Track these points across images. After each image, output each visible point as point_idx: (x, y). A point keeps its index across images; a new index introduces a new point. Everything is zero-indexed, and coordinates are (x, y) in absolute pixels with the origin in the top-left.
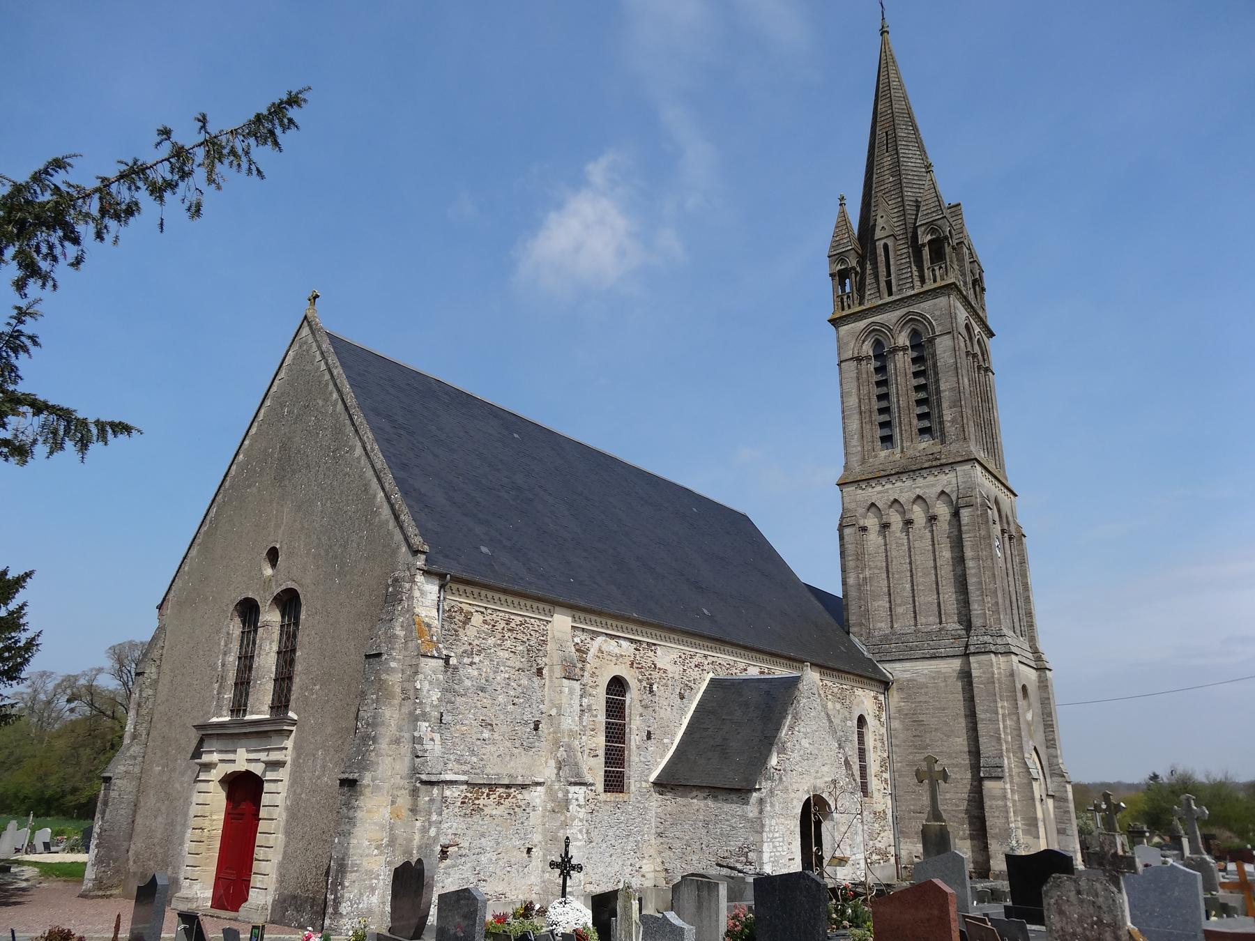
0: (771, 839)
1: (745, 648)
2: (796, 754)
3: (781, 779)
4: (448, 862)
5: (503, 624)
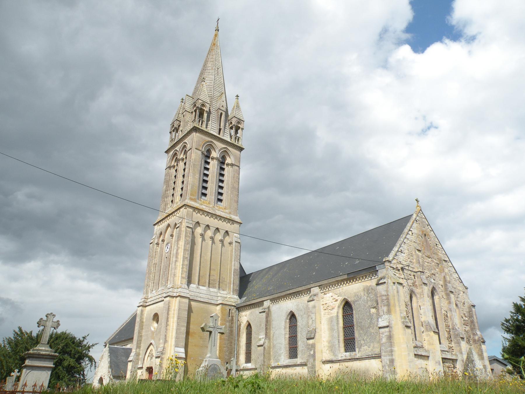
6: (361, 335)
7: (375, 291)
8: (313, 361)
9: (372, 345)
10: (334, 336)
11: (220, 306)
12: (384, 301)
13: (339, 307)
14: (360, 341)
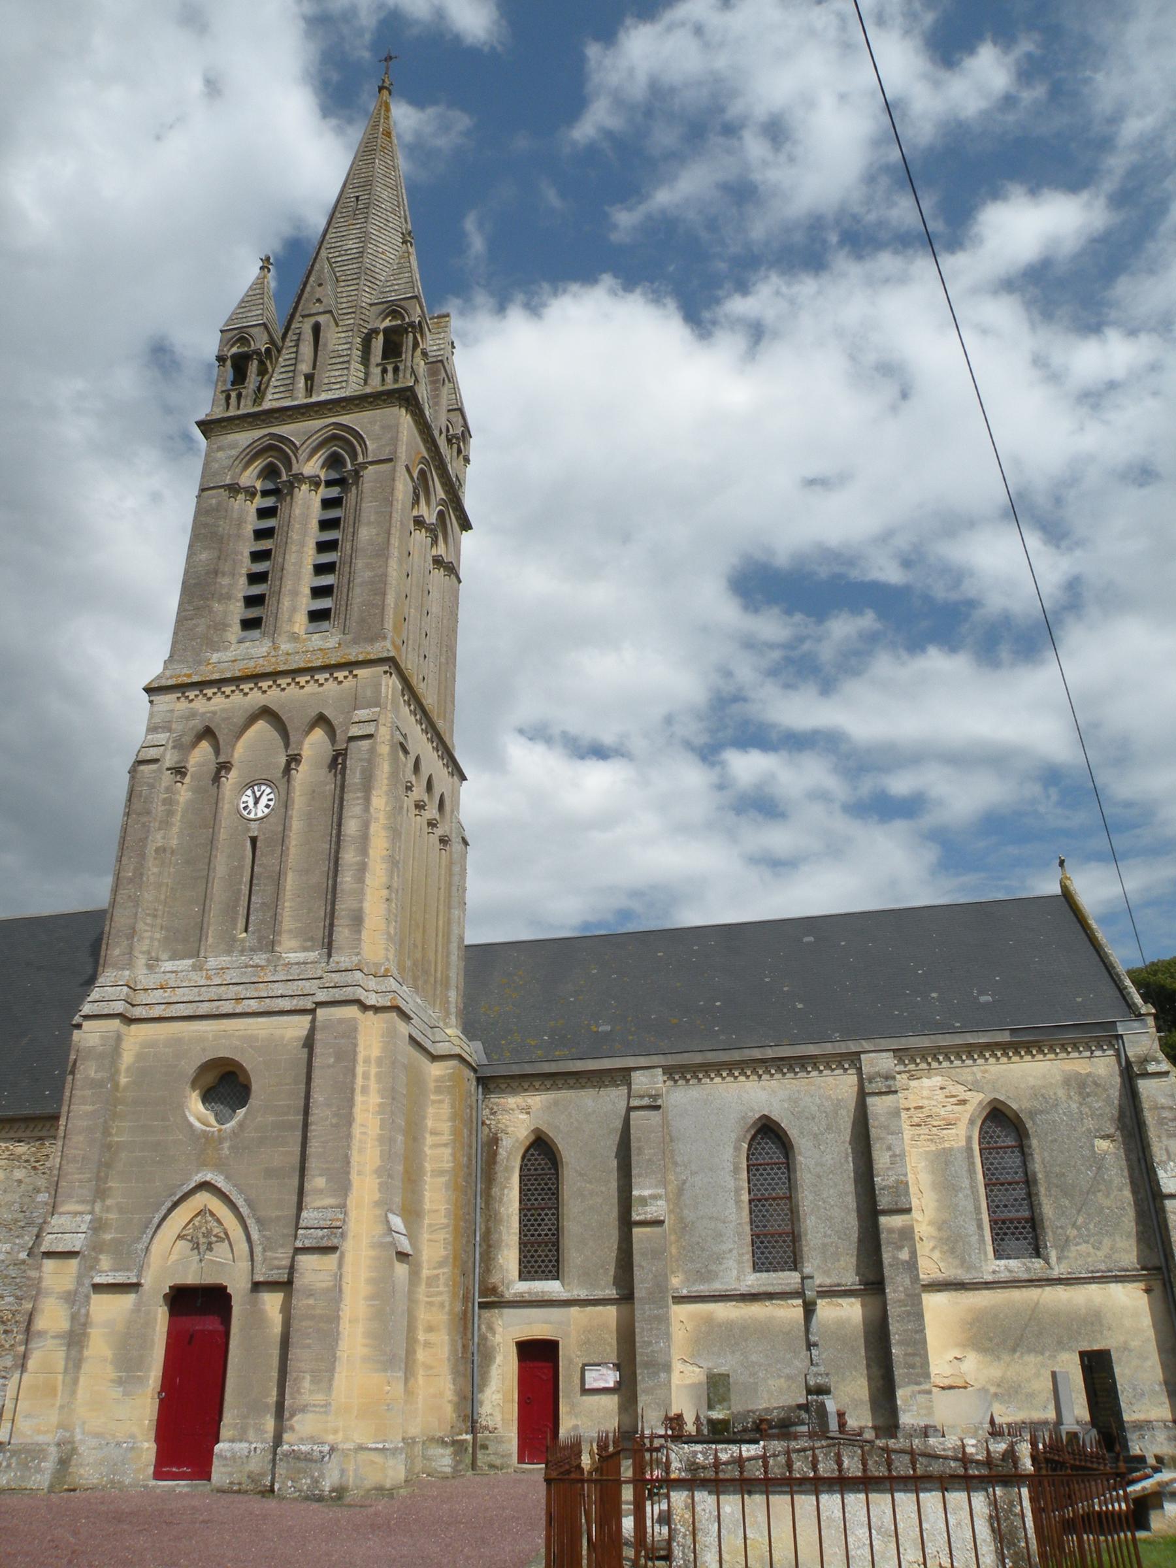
6: (1063, 1212)
7: (1107, 1090)
8: (911, 1282)
9: (1107, 1242)
10: (960, 1208)
11: (453, 1063)
12: (1167, 1124)
13: (972, 1122)
14: (1061, 1227)
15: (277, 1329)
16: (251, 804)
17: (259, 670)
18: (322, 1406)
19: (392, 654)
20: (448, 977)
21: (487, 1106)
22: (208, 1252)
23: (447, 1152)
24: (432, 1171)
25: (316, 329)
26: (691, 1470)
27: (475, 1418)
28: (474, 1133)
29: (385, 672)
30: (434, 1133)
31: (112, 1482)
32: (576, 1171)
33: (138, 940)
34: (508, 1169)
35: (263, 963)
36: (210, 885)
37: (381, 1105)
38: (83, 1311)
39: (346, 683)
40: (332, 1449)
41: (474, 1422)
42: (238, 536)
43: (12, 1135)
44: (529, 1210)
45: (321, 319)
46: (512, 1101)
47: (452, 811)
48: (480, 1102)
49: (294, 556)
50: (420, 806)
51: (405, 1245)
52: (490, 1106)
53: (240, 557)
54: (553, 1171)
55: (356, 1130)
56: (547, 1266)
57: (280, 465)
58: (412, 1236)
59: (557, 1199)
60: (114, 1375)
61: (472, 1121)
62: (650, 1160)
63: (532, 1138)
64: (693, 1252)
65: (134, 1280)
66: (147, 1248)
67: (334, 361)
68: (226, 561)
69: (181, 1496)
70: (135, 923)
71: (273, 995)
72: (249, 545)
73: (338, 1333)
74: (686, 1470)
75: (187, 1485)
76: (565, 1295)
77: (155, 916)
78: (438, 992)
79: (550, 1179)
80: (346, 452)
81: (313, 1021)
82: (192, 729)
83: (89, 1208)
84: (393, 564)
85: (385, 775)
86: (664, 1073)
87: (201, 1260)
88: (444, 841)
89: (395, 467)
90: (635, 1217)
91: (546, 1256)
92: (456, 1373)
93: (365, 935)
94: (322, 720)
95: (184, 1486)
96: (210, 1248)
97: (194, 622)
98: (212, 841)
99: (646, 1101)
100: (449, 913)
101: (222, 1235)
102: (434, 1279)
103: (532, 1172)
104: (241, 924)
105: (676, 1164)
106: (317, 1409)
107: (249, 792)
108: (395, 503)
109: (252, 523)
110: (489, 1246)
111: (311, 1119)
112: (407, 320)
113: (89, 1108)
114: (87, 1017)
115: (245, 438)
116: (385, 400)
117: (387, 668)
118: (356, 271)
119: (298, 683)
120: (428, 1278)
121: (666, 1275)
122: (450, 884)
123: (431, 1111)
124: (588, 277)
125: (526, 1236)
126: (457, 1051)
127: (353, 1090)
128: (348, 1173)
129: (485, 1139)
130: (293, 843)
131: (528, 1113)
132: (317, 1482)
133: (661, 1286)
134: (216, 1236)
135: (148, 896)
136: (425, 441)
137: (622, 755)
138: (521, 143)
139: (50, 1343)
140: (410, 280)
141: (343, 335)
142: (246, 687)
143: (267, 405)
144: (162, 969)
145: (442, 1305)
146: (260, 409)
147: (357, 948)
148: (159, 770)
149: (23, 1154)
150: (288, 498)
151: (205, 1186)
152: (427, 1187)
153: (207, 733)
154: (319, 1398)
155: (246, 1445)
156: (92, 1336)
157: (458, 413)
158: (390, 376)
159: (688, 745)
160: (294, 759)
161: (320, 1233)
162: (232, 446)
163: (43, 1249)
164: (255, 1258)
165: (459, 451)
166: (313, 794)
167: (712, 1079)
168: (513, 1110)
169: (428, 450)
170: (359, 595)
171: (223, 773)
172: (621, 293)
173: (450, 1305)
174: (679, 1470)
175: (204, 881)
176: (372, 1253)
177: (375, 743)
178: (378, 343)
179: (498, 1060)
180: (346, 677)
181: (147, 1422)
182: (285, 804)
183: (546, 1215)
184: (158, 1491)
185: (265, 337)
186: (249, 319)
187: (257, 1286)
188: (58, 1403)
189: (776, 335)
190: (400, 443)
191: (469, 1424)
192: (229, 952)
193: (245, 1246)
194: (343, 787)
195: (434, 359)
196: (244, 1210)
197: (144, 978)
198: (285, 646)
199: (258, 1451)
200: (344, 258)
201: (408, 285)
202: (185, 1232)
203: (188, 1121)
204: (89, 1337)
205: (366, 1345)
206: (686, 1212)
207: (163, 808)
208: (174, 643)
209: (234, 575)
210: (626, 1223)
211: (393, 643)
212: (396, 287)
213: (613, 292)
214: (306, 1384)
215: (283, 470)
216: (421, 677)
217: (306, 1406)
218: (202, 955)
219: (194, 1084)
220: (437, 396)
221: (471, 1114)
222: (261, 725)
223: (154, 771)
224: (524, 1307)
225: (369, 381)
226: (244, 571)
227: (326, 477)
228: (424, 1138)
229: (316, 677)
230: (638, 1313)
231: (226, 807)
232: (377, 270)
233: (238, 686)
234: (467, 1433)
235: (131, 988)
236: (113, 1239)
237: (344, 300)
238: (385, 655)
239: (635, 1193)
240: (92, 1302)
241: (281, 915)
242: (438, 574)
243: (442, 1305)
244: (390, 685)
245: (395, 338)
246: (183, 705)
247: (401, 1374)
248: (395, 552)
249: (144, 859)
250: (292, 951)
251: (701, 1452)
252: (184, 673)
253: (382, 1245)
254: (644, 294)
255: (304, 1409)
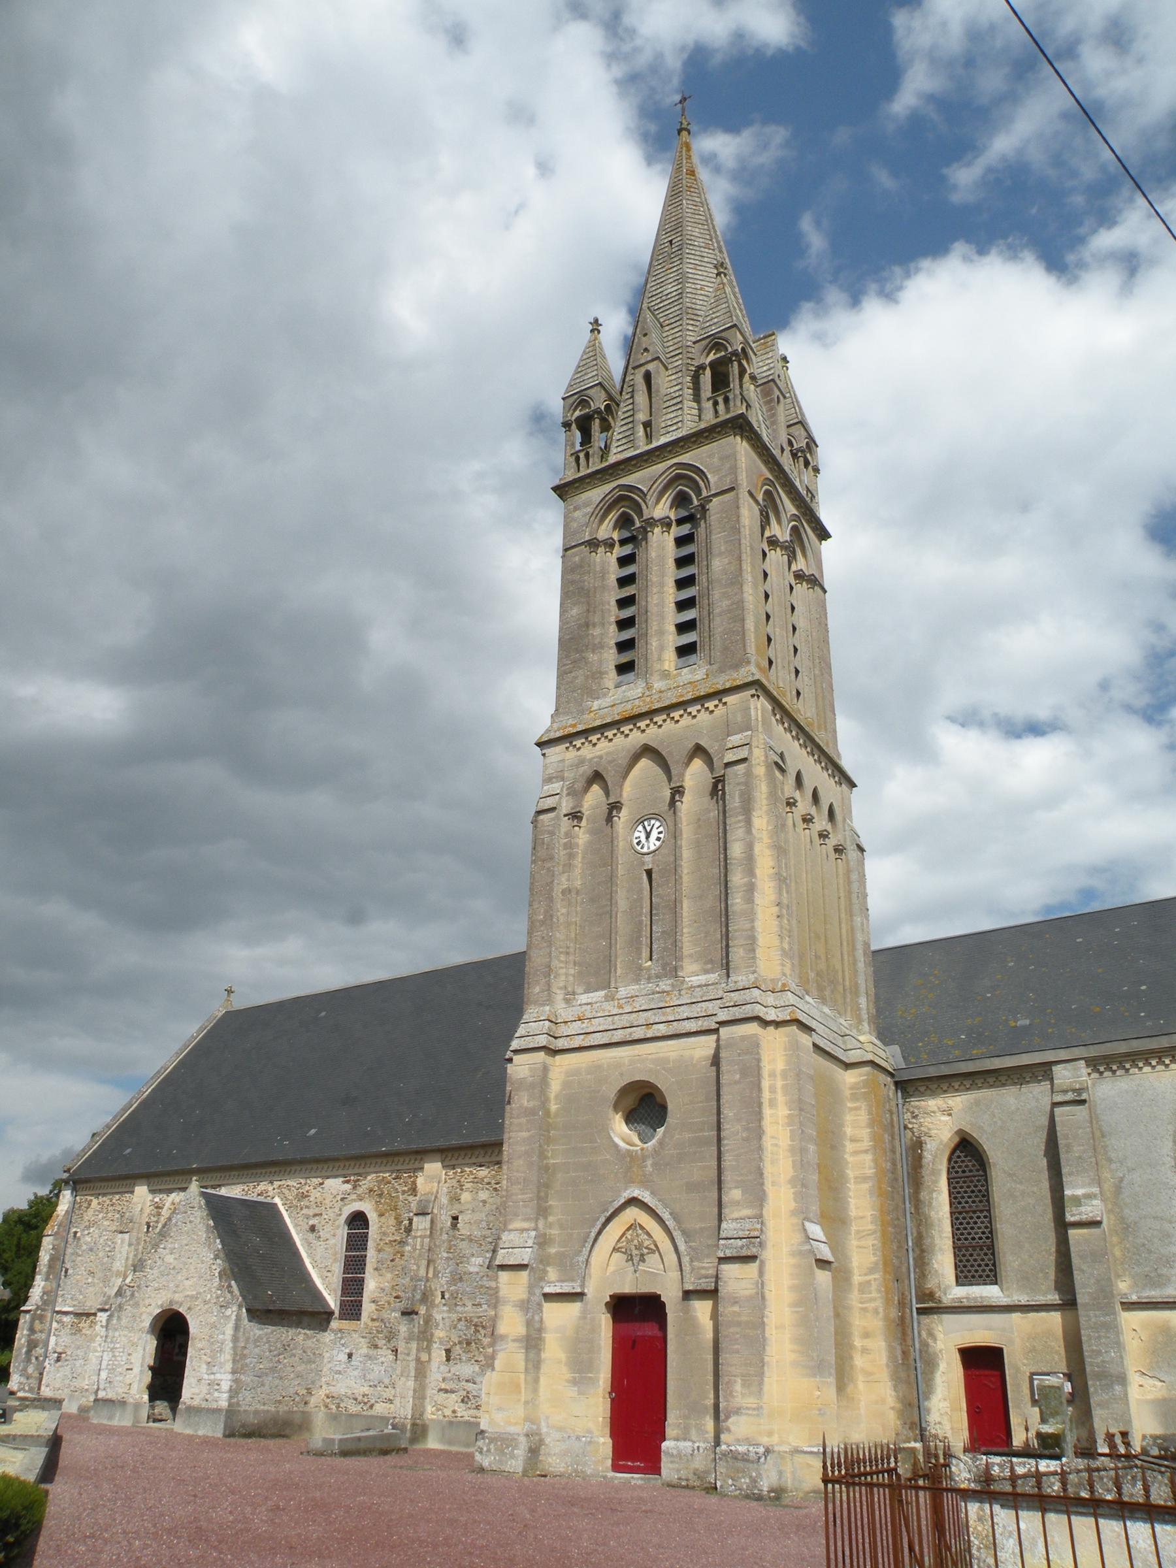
0: (112, 1349)
1: (317, 1161)
2: (155, 1271)
3: (132, 1295)
4: (59, 1363)
5: (108, 1202)
15: (710, 1335)
16: (643, 839)
17: (636, 711)
18: (754, 1409)
19: (756, 678)
20: (856, 984)
21: (908, 1110)
22: (641, 1263)
23: (868, 1158)
24: (856, 1178)
25: (648, 377)
26: (980, 1481)
27: (923, 1425)
28: (897, 1137)
29: (753, 696)
30: (853, 1140)
31: (576, 1471)
32: (1005, 1172)
33: (555, 977)
34: (936, 1173)
35: (668, 988)
36: (613, 920)
37: (789, 1116)
38: (537, 1318)
39: (717, 712)
40: (768, 1451)
41: (922, 1430)
42: (603, 587)
43: (473, 1160)
44: (960, 1213)
45: (650, 367)
46: (932, 1103)
47: (844, 820)
48: (900, 1106)
49: (656, 596)
50: (808, 820)
51: (826, 1253)
52: (912, 1110)
53: (607, 607)
54: (981, 1173)
55: (767, 1143)
56: (984, 1271)
57: (632, 513)
58: (835, 1242)
59: (988, 1201)
60: (569, 1376)
61: (893, 1126)
62: (1080, 1157)
63: (957, 1140)
64: (1140, 1255)
65: (579, 1290)
66: (587, 1261)
67: (668, 404)
68: (595, 612)
69: (636, 1487)
70: (550, 962)
71: (679, 1018)
72: (614, 594)
73: (764, 1339)
74: (975, 1481)
75: (642, 1479)
76: (1005, 1301)
77: (567, 953)
78: (848, 1000)
79: (978, 1181)
80: (631, 509)
81: (718, 1040)
82: (582, 775)
83: (533, 1225)
84: (748, 589)
85: (764, 796)
86: (1088, 1066)
87: (635, 1271)
88: (839, 850)
89: (737, 494)
90: (1070, 1218)
91: (983, 1260)
92: (897, 1380)
93: (760, 953)
94: (699, 750)
95: (638, 1479)
96: (642, 1259)
97: (573, 674)
98: (612, 877)
99: (1070, 1096)
100: (852, 921)
101: (652, 1247)
102: (864, 1287)
103: (960, 1174)
104: (645, 953)
105: (1110, 1160)
106: (750, 1412)
107: (640, 828)
108: (742, 529)
109: (614, 572)
110: (923, 1251)
111: (723, 1134)
112: (730, 350)
113: (525, 1134)
114: (516, 1052)
115: (596, 494)
116: (719, 432)
117: (753, 692)
118: (678, 312)
119: (690, 713)
120: (860, 1284)
121: (1109, 1279)
122: (850, 892)
123: (849, 1118)
124: (937, 248)
125: (959, 1239)
126: (870, 1057)
127: (760, 1105)
128: (763, 1184)
129: (909, 1143)
130: (685, 871)
131: (950, 1115)
132: (755, 1481)
133: (1105, 1293)
134: (646, 1248)
135: (560, 935)
136: (766, 463)
137: (1061, 729)
138: (842, 136)
139: (512, 1346)
140: (728, 310)
141: (673, 377)
142: (626, 729)
143: (612, 459)
144: (579, 1002)
145: (876, 1311)
146: (607, 464)
147: (752, 966)
148: (557, 817)
149: (486, 1177)
150: (644, 543)
151: (633, 1201)
152: (851, 1194)
153: (597, 777)
154: (750, 1401)
155: (690, 1444)
156: (547, 1340)
157: (799, 426)
158: (721, 407)
159: (1129, 708)
160: (678, 792)
161: (739, 1243)
162: (586, 505)
163: (497, 1263)
164: (684, 1268)
165: (807, 464)
166: (698, 822)
167: (1141, 1069)
168: (934, 1112)
169: (771, 470)
170: (719, 625)
171: (614, 813)
172: (976, 257)
173: (884, 1310)
174: (968, 1480)
175: (608, 916)
176: (793, 1261)
177: (750, 766)
178: (707, 378)
179: (916, 1063)
180: (716, 706)
181: (601, 1419)
182: (674, 834)
183: (979, 1217)
184: (616, 1482)
185: (603, 395)
186: (586, 382)
187: (688, 1295)
188: (523, 1399)
189: (1153, 262)
190: (739, 470)
191: (918, 1432)
192: (637, 980)
193: (674, 1257)
194: (724, 812)
195: (765, 380)
196: (671, 1223)
197: (563, 1012)
198: (658, 685)
199: (701, 1451)
200: (666, 303)
201: (726, 316)
202: (619, 1245)
203: (613, 1141)
204: (544, 1341)
205: (792, 1351)
206: (1127, 1211)
207: (565, 852)
208: (558, 697)
209: (603, 624)
210: (1062, 1226)
211: (758, 666)
212: (716, 320)
213: (966, 259)
214: (738, 1387)
215: (636, 517)
216: (794, 693)
217: (739, 1409)
218: (613, 985)
219: (616, 1107)
220: (774, 415)
221: (892, 1120)
222: (644, 763)
223: (553, 819)
224: (964, 1313)
225: (703, 417)
226: (613, 619)
227: (676, 516)
228: (844, 1146)
229: (689, 710)
230: (1083, 1320)
231: (621, 844)
232: (698, 307)
233: (618, 729)
234: (915, 1441)
235: (552, 1022)
236: (557, 1253)
237: (671, 343)
238: (750, 679)
239: (1068, 1192)
240: (544, 1310)
241: (681, 941)
242: (801, 589)
243: (876, 1311)
244: (760, 707)
245: (721, 369)
246: (572, 754)
247: (832, 1380)
248: (748, 577)
249: (552, 901)
250: (694, 975)
251: (998, 1464)
252: (571, 724)
253: (801, 1254)
254: (1001, 253)
255: (738, 1411)
